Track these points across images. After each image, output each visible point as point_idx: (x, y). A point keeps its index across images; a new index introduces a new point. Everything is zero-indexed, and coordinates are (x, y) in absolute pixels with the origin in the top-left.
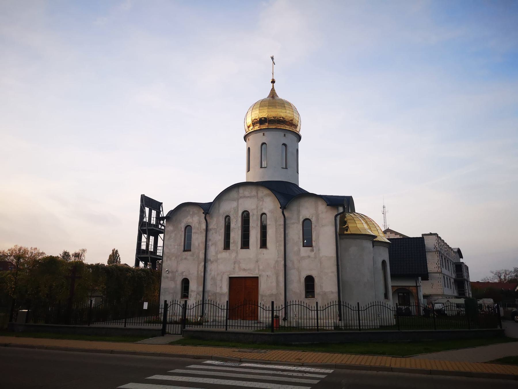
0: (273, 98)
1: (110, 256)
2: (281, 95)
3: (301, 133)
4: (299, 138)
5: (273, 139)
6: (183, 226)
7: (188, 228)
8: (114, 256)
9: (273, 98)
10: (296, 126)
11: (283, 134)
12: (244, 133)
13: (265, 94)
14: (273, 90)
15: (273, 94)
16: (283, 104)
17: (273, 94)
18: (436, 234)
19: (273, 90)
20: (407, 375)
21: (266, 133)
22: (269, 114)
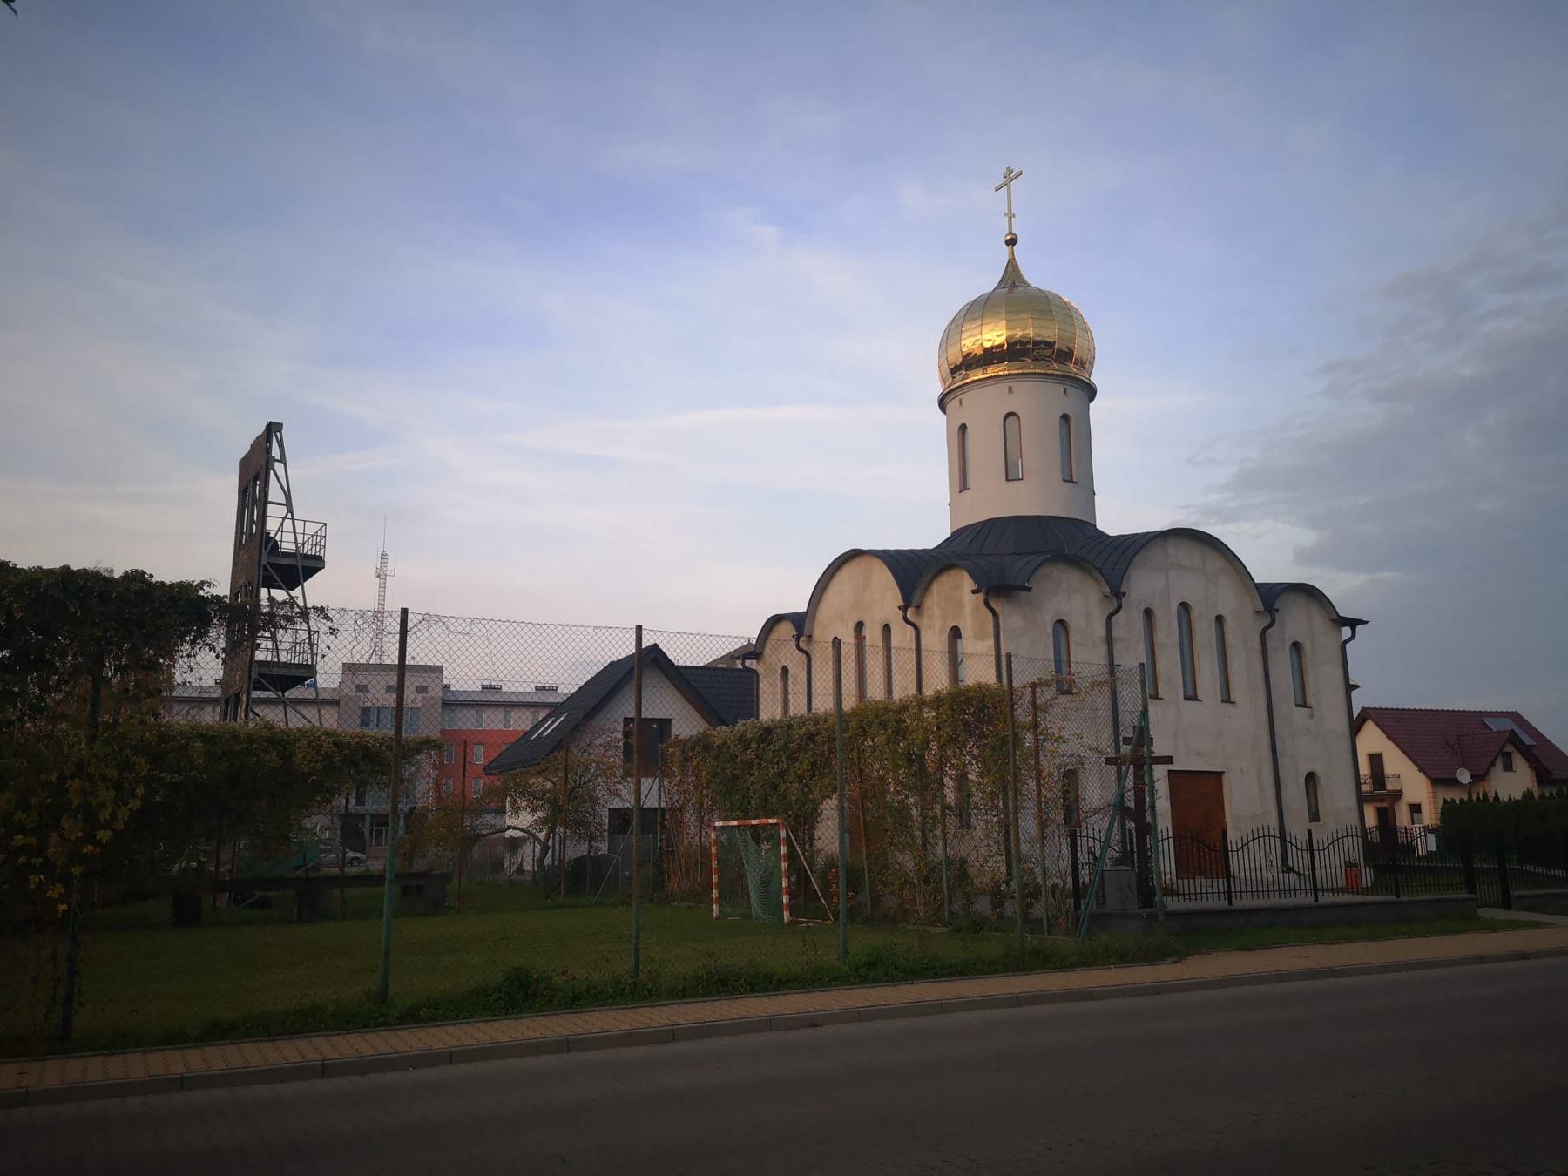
0: (1012, 291)
1: (66, 568)
2: (1037, 276)
3: (1095, 378)
4: (1091, 392)
5: (1034, 400)
6: (1047, 619)
7: (1061, 625)
8: (112, 571)
9: (1012, 291)
10: (1085, 364)
11: (1060, 388)
12: (938, 389)
13: (988, 281)
14: (1012, 266)
15: (1012, 276)
16: (1045, 305)
17: (1012, 276)
18: (854, 555)
19: (1012, 266)
20: (1545, 918)
21: (1071, 390)
22: (1019, 333)
